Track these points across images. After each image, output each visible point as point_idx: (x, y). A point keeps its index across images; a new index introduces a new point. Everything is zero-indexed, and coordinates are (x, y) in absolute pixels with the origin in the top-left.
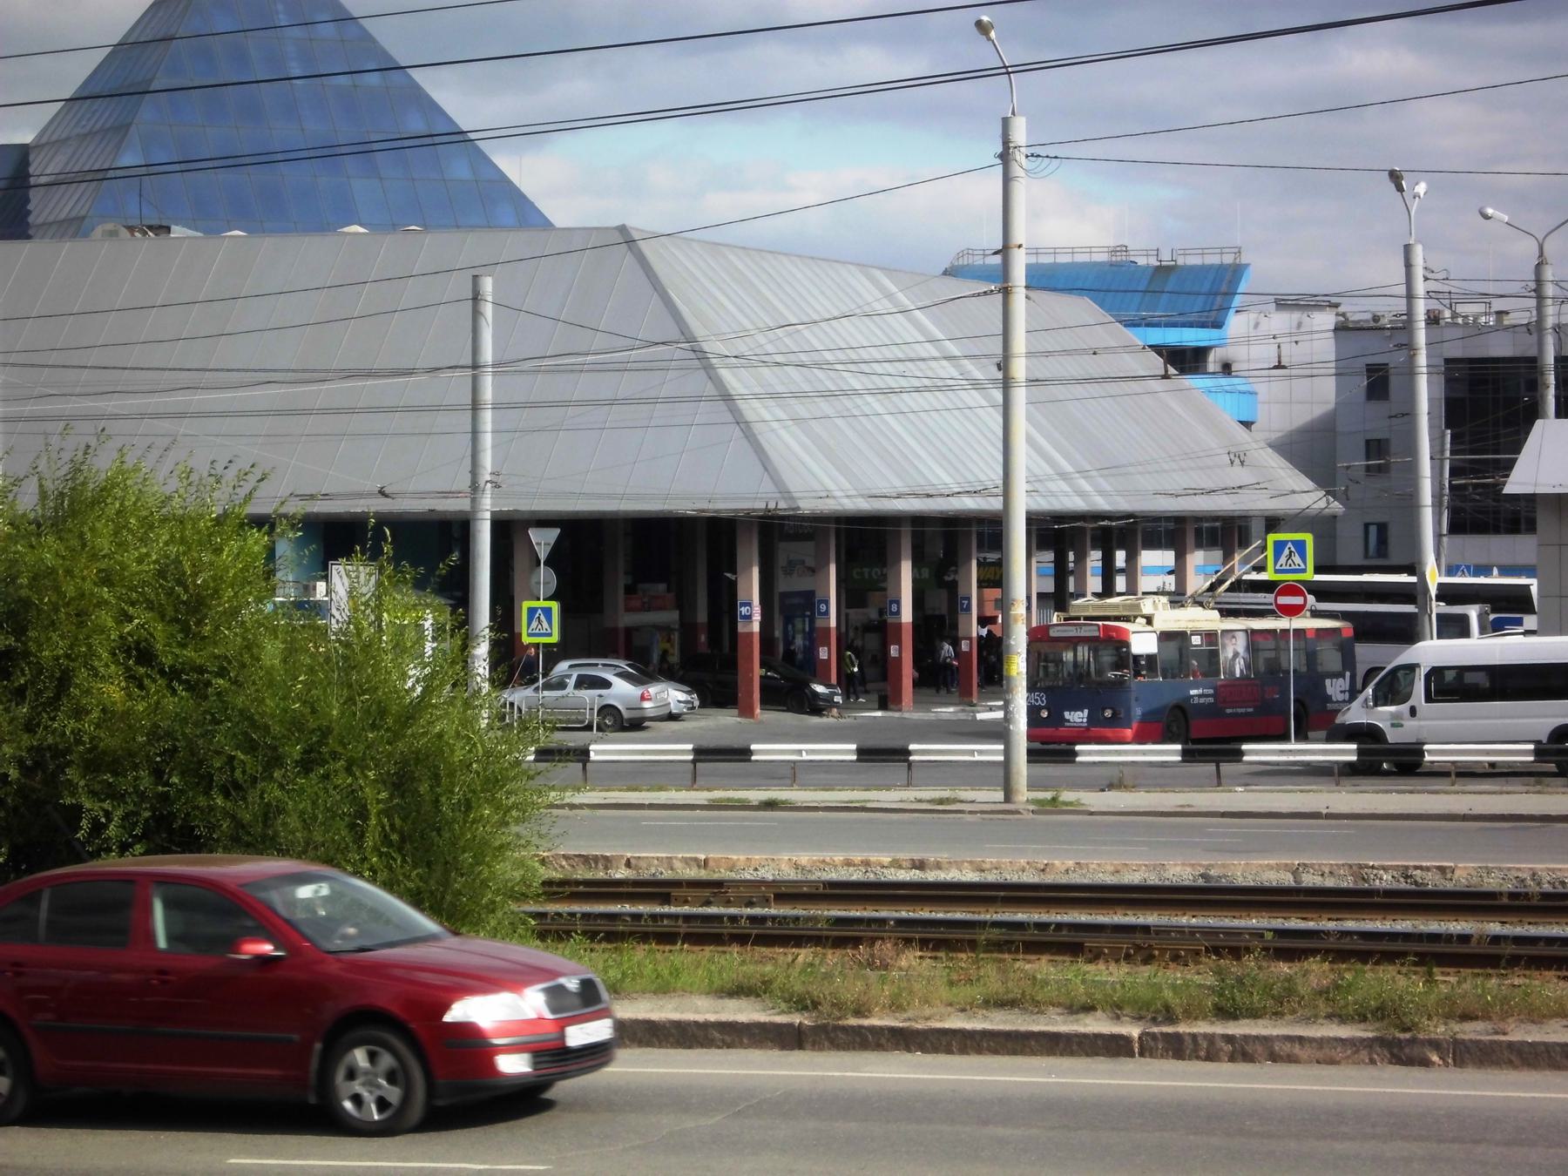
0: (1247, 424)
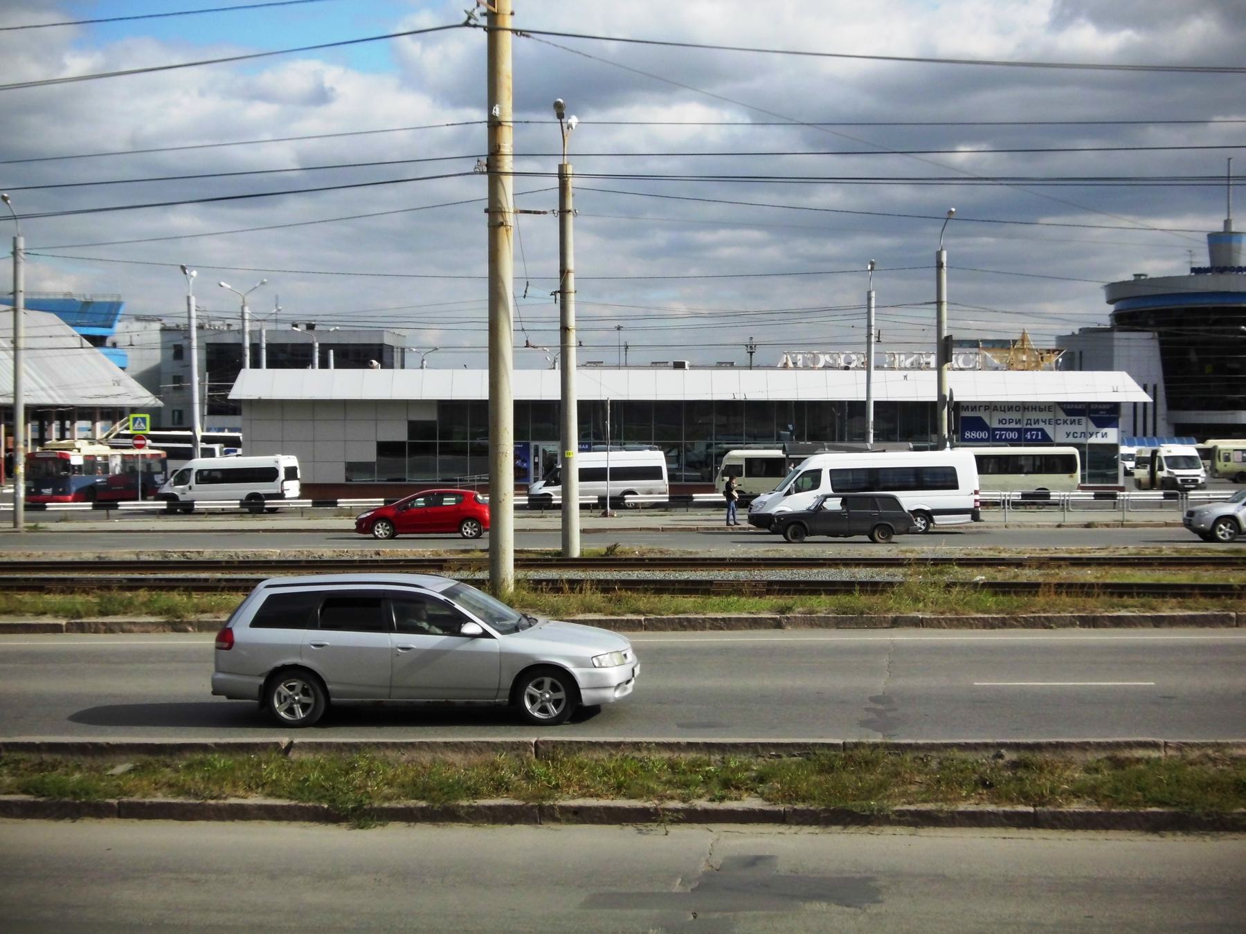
0: (123, 368)
